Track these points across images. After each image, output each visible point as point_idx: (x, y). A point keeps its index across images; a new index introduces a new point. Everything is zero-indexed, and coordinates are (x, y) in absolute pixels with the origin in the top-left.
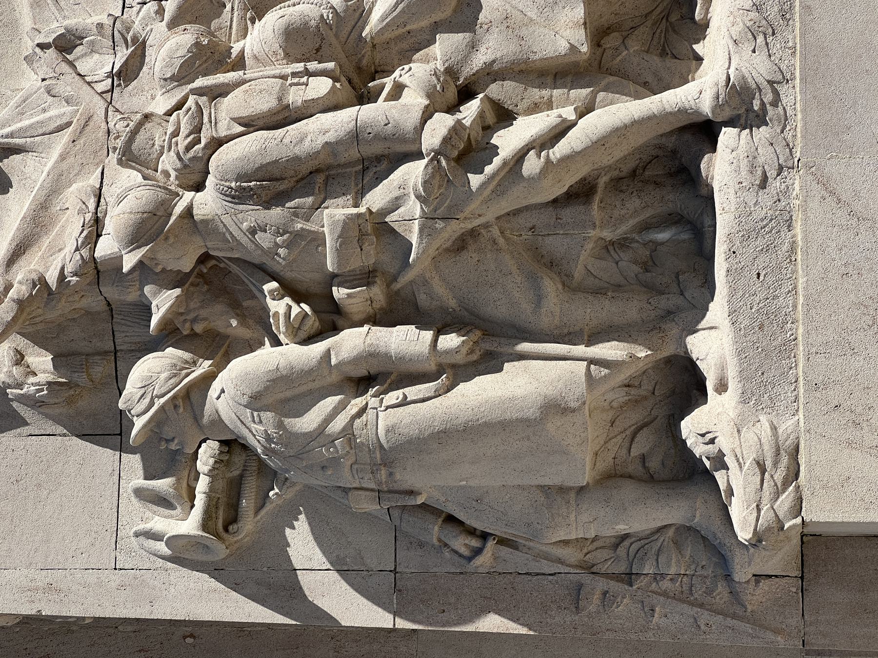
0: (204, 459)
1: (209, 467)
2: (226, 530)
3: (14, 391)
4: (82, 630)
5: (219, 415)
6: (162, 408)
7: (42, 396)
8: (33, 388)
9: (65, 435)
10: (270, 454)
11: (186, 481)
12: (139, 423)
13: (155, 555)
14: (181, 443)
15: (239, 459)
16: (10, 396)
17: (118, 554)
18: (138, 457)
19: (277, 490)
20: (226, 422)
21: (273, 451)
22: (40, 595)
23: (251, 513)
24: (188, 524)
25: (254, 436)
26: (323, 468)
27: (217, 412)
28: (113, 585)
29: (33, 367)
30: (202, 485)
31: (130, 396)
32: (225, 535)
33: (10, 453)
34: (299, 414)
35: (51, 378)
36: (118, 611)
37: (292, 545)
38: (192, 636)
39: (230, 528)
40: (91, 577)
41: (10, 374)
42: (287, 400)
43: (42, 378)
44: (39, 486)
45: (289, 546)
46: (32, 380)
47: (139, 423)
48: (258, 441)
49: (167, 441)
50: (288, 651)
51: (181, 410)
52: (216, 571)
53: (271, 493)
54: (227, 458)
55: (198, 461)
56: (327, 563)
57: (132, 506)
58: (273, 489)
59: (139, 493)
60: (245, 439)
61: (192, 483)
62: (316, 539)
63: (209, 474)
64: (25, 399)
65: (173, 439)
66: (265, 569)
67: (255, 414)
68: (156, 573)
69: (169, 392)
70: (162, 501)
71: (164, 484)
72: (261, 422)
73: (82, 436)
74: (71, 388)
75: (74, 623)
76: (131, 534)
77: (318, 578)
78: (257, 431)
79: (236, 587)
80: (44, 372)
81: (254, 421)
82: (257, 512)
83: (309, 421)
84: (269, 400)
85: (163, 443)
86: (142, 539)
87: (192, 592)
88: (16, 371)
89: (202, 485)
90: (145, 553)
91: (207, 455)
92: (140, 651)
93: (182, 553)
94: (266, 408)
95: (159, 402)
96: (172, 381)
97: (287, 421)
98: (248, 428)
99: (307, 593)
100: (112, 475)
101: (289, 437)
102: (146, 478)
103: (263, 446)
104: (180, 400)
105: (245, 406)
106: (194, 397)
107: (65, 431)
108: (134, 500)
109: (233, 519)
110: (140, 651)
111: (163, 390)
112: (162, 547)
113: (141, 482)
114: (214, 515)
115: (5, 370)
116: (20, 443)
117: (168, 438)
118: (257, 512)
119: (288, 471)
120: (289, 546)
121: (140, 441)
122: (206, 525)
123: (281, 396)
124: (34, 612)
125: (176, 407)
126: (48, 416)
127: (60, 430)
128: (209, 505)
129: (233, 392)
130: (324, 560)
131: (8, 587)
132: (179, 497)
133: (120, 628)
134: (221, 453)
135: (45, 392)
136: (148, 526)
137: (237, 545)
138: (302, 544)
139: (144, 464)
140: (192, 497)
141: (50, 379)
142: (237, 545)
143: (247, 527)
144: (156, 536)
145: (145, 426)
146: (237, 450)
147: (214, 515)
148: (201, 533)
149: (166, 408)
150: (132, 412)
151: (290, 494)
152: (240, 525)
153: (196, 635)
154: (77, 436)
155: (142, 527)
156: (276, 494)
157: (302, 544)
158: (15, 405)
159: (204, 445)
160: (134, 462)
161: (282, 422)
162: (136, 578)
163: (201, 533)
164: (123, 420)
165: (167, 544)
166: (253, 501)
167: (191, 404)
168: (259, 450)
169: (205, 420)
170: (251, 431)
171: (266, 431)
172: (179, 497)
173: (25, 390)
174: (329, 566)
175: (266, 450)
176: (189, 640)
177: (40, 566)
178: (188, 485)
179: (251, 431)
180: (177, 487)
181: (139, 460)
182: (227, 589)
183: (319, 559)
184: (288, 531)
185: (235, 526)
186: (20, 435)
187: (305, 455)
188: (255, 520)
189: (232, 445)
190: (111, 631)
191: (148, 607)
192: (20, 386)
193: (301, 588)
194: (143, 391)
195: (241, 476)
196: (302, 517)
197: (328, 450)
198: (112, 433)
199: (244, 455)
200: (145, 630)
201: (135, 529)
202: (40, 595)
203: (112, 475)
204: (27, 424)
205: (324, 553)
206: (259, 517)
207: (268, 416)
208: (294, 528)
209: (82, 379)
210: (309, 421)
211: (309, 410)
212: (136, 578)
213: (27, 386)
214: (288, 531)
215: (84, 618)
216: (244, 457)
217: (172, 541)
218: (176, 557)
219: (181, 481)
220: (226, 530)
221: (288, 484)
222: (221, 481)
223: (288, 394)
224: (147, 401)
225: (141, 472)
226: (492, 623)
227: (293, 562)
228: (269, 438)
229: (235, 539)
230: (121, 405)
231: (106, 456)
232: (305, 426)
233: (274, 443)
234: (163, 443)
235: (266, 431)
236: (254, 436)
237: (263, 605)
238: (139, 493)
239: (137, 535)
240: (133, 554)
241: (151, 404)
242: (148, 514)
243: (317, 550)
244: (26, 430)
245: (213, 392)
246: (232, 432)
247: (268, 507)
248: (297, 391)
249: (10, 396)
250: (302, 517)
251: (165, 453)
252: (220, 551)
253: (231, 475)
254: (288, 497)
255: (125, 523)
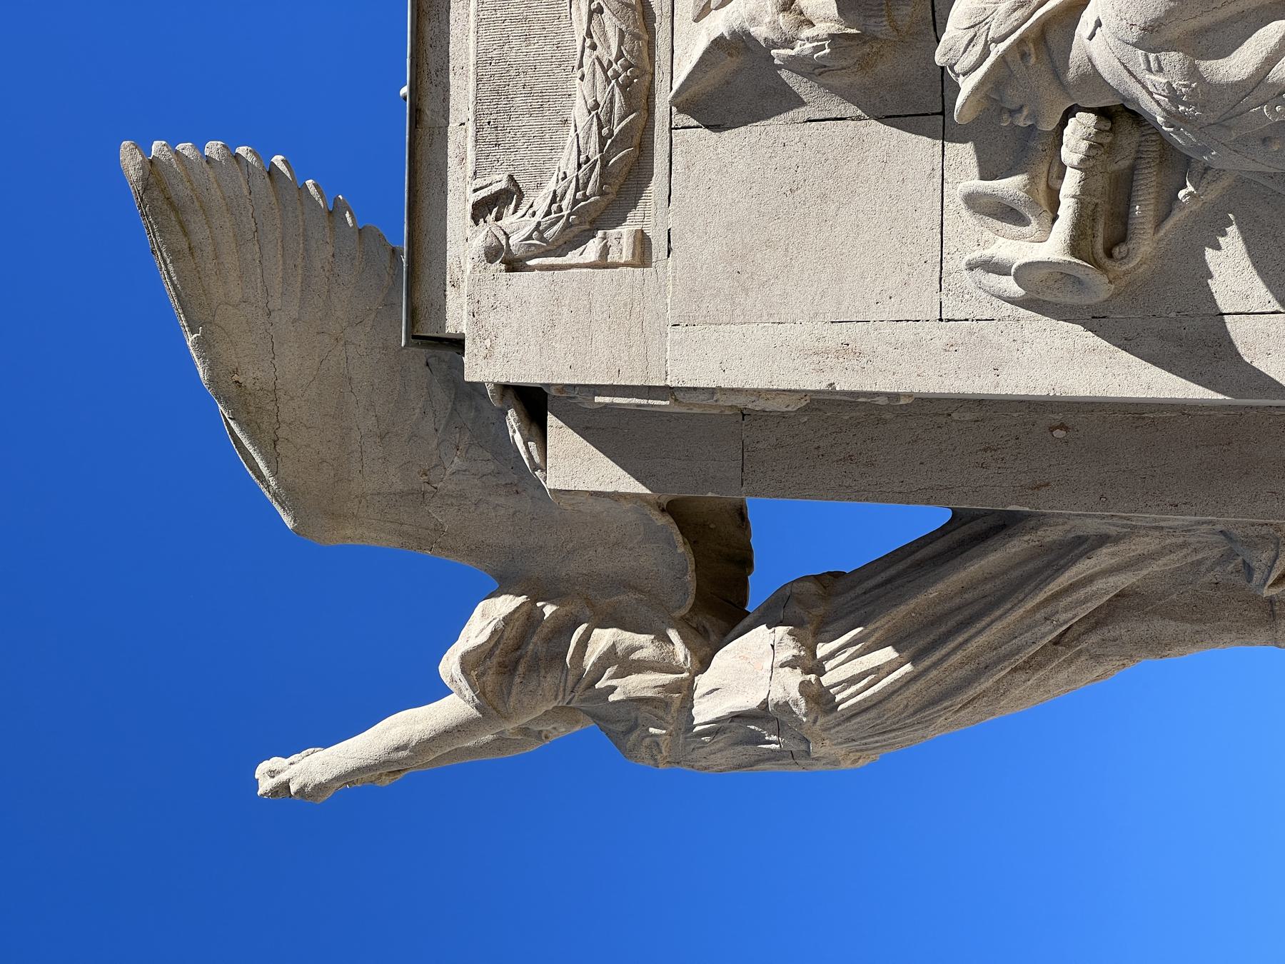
0: (1073, 142)
1: (1081, 156)
2: (1109, 254)
3: (782, 51)
4: (899, 419)
5: (1093, 66)
6: (1003, 58)
7: (823, 57)
8: (809, 45)
9: (859, 118)
10: (1177, 123)
11: (1044, 180)
12: (967, 85)
13: (999, 297)
14: (1034, 115)
15: (1129, 139)
16: (777, 61)
17: (944, 297)
18: (969, 147)
19: (1190, 188)
20: (1106, 76)
21: (1182, 118)
22: (831, 361)
23: (1149, 228)
24: (1051, 245)
25: (1151, 94)
26: (1265, 140)
27: (1090, 60)
28: (939, 344)
29: (808, 13)
30: (1071, 184)
31: (952, 43)
32: (1108, 263)
33: (779, 149)
34: (1224, 52)
35: (835, 28)
36: (947, 382)
37: (1216, 275)
38: (1062, 427)
39: (1116, 251)
40: (906, 332)
41: (774, 25)
42: (1204, 31)
43: (822, 29)
44: (824, 196)
45: (1211, 277)
46: (807, 32)
47: (967, 85)
48: (1159, 104)
49: (1012, 112)
50: (1215, 448)
51: (1033, 60)
52: (1095, 320)
53: (1182, 194)
54: (1109, 139)
55: (1063, 148)
56: (1274, 302)
57: (962, 222)
58: (1185, 186)
59: (972, 201)
60: (1135, 101)
61: (1053, 183)
62: (1255, 264)
63: (1083, 166)
64: (795, 64)
65: (1020, 109)
66: (1173, 315)
67: (1152, 56)
68: (1001, 325)
69: (1012, 32)
70: (1008, 213)
71: (1011, 186)
72: (1160, 70)
73: (886, 119)
74: (865, 43)
75: (887, 408)
76: (963, 265)
77: (1260, 326)
78: (1153, 86)
79: (1127, 343)
80: (825, 20)
81: (1150, 70)
82: (1158, 225)
83: (1239, 64)
84: (1174, 32)
85: (1005, 116)
86: (979, 273)
87: (1059, 354)
88: (784, 20)
89: (1071, 184)
90: (984, 295)
91: (1078, 134)
92: (985, 450)
93: (1043, 293)
94: (1169, 46)
95: (997, 50)
96: (1018, 14)
97: (1204, 65)
98: (1139, 82)
99: (1241, 350)
100: (931, 176)
101: (1207, 93)
102: (982, 178)
103: (1164, 110)
104: (1031, 45)
105: (1134, 45)
106: (1054, 37)
107: (859, 112)
108: (966, 214)
109: (1120, 236)
110: (985, 450)
111: (1003, 30)
112: (1010, 285)
113: (974, 183)
114: (1089, 232)
115: (767, 20)
116: (794, 133)
117: (1013, 107)
118: (1158, 225)
119: (1206, 151)
120: (1211, 277)
121: (969, 116)
122: (1077, 245)
123: (1194, 24)
124: (823, 386)
125: (1024, 56)
126: (833, 90)
127: (852, 110)
128: (1081, 215)
129: (1114, 22)
130: (1270, 297)
131: (785, 350)
132: (1034, 203)
133: (955, 416)
134: (1100, 131)
135: (827, 51)
136: (987, 253)
137: (1127, 278)
138: (1231, 272)
139: (979, 158)
140: (1054, 204)
141: (833, 31)
142: (1127, 278)
143: (1143, 249)
144: (998, 268)
145: (976, 90)
146: (1125, 125)
147: (1089, 232)
148: (1068, 258)
149: (1009, 59)
150: (956, 68)
151: (1213, 192)
152: (1131, 246)
153: (1069, 425)
154: (877, 119)
155: (977, 254)
156: (1190, 194)
157: (1231, 272)
158: (784, 74)
159: (1072, 121)
160: (963, 155)
161: (1196, 68)
162: (971, 333)
163: (1068, 258)
164: (944, 81)
165: (1016, 279)
166: (1152, 207)
167: (1049, 50)
168: (1160, 119)
169: (1072, 74)
170: (1144, 87)
171: (1169, 84)
172: (1034, 203)
173: (797, 49)
174: (1277, 307)
175: (1171, 117)
176: (1059, 433)
177: (829, 318)
178: (1048, 186)
179: (1144, 87)
180: (1030, 189)
181: (972, 152)
182: (1112, 347)
183: (1261, 296)
184: (1209, 253)
185: (1123, 248)
186: (793, 121)
187: (1234, 121)
188: (1157, 237)
189: (1118, 116)
190: (942, 420)
191: (992, 376)
192: (789, 43)
193: (1231, 342)
194: (971, 33)
195: (1133, 169)
196: (1233, 230)
197: (1272, 110)
198: (930, 111)
199: (1137, 135)
200: (991, 419)
201: (967, 257)
202: (831, 361)
203: (931, 176)
204: (803, 104)
205: (1268, 286)
206: (1162, 233)
207: (1172, 59)
208: (1219, 248)
209: (882, 28)
210: (1239, 64)
211: (1241, 44)
212: (971, 333)
213: (800, 42)
214: (1209, 253)
215: (897, 396)
216: (1136, 137)
217: (1025, 273)
218: (1032, 300)
219: (1037, 180)
220: (1109, 254)
221: (1209, 176)
222: (1099, 177)
223: (1206, 20)
224: (977, 49)
225: (976, 171)
226: (710, 494)
227: (1219, 302)
228: (1174, 97)
229: (1124, 268)
230: (939, 59)
231: (921, 147)
232: (1234, 71)
233: (1183, 104)
234: (1005, 116)
235: (1169, 84)
236: (1151, 94)
237: (1170, 371)
238: (972, 201)
239: (971, 267)
240: (967, 297)
241: (985, 53)
242: (988, 235)
243: (1259, 283)
244: (801, 113)
245: (1083, 29)
246: (1115, 92)
247: (1177, 217)
248: (1221, 14)
249: (777, 61)
250: (1233, 230)
251: (1010, 136)
252: (1101, 287)
253: (1115, 167)
254: (1210, 197)
255: (953, 250)
